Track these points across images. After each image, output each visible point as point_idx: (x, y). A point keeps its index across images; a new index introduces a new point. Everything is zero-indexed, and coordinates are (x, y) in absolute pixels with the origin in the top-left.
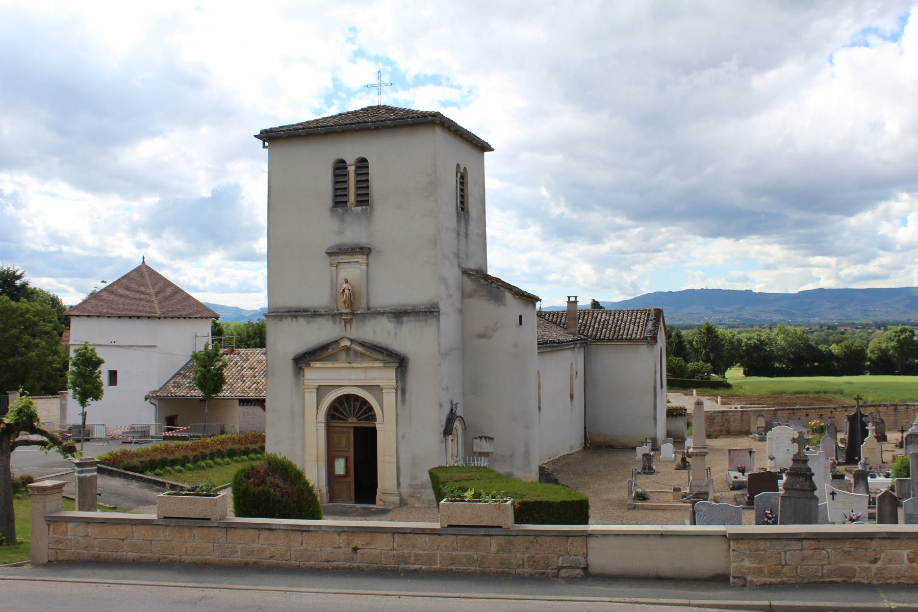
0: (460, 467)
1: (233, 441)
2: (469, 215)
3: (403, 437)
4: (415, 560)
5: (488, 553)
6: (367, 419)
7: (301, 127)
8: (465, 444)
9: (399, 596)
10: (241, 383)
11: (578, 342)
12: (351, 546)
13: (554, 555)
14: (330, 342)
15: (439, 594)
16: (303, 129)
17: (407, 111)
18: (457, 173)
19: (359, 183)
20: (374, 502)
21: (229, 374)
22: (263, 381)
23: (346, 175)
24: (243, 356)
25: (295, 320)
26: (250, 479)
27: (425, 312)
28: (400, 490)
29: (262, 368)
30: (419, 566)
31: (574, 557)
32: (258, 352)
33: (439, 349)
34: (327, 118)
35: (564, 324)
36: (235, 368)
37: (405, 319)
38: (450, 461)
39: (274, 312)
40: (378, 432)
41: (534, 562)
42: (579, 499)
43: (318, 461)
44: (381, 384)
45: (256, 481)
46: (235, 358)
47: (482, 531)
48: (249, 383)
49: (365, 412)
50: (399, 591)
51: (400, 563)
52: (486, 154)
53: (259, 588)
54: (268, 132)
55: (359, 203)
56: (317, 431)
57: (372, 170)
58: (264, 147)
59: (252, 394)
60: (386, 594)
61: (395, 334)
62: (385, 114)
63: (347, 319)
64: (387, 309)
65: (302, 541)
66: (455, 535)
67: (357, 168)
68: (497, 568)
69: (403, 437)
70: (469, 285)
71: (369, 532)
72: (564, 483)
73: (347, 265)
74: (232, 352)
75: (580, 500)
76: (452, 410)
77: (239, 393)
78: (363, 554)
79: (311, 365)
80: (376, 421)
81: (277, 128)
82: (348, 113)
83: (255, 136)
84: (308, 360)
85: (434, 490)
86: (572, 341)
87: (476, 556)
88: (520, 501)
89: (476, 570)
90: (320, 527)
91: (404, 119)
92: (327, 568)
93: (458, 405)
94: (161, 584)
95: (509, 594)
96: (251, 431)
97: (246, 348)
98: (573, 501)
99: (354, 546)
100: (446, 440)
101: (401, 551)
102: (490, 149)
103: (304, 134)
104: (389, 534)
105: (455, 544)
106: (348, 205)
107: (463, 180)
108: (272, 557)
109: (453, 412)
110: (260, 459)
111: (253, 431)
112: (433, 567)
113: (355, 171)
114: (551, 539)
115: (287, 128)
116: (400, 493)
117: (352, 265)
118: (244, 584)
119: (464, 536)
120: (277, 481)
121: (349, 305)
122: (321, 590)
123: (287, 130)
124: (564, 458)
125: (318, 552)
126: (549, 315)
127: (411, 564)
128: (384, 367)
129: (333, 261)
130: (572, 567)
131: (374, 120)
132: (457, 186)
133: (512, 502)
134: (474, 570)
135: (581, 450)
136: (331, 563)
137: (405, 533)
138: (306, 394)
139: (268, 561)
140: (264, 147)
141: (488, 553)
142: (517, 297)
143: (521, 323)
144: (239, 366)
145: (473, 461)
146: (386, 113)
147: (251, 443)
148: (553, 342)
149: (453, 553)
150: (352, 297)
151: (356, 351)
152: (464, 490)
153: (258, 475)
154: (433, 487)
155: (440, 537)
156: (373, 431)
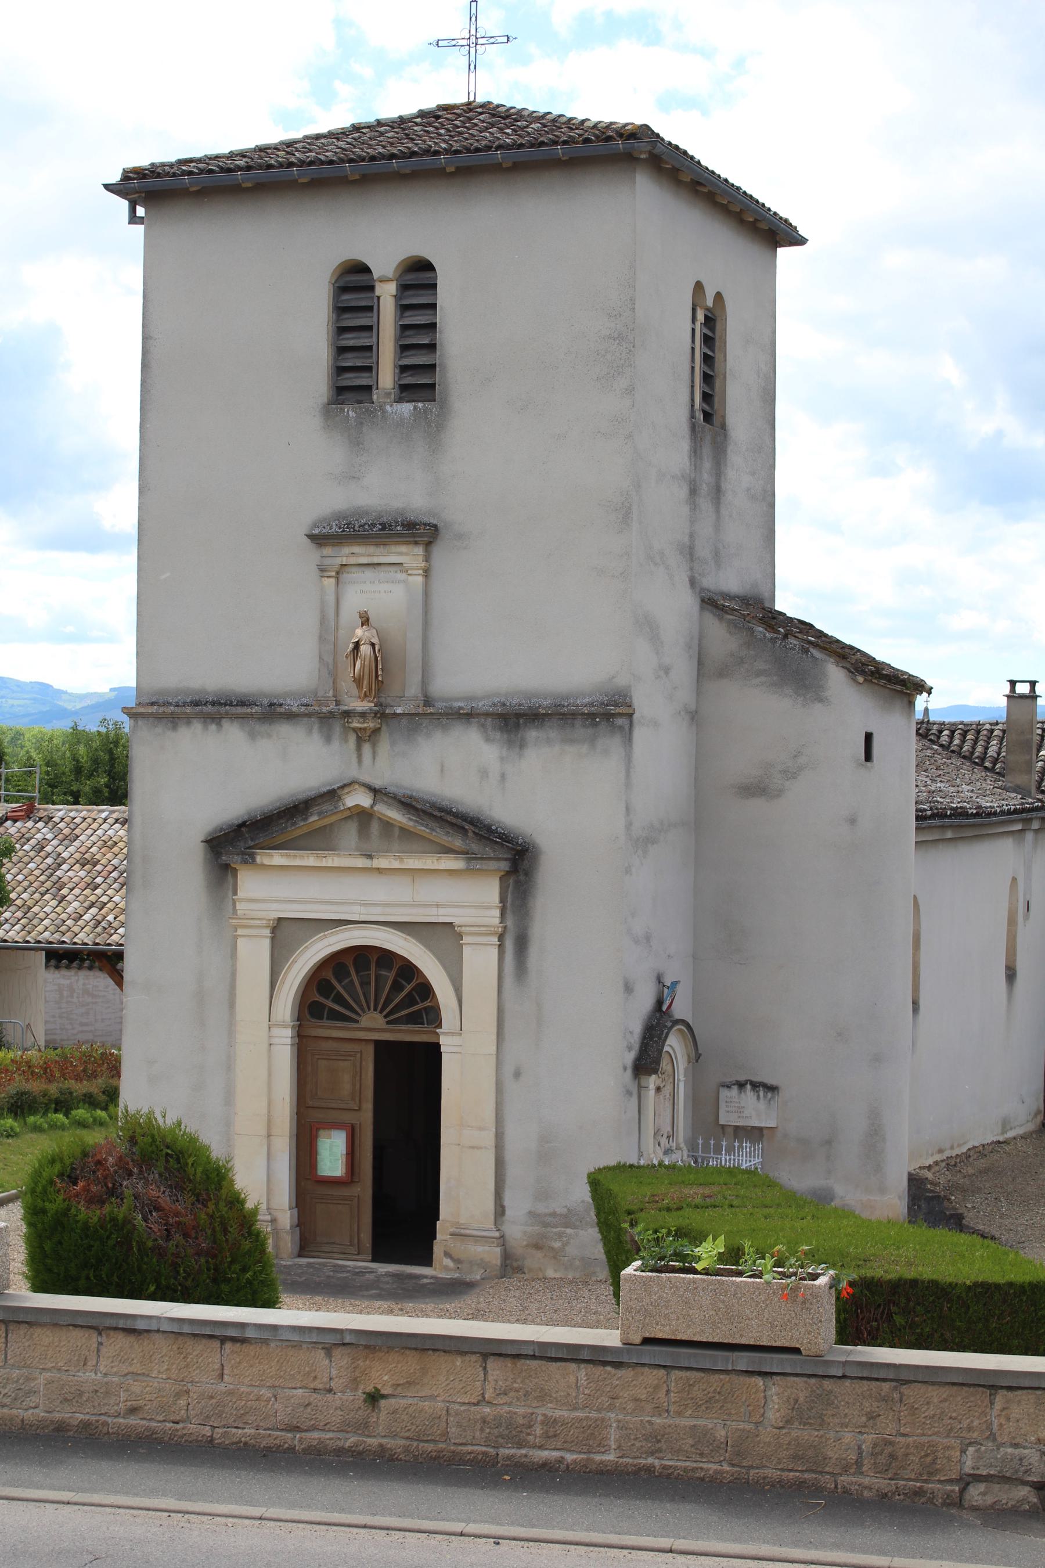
0: (680, 1169)
1: (28, 1069)
2: (725, 436)
3: (517, 1074)
4: (547, 1436)
5: (757, 1424)
6: (414, 1019)
7: (241, 163)
8: (696, 1101)
9: (497, 1540)
10: (54, 903)
11: (1034, 814)
12: (362, 1387)
13: (951, 1441)
14: (312, 793)
15: (614, 1539)
16: (249, 168)
17: (554, 121)
18: (694, 310)
19: (408, 333)
20: (427, 1259)
21: (20, 877)
22: (116, 899)
23: (370, 309)
24: (62, 825)
25: (213, 727)
26: (75, 1184)
27: (592, 716)
28: (503, 1228)
29: (115, 862)
30: (556, 1454)
31: (1010, 1450)
32: (106, 813)
33: (629, 826)
34: (318, 137)
35: (995, 761)
36: (38, 859)
37: (532, 734)
38: (651, 1151)
39: (153, 704)
40: (445, 1059)
41: (892, 1456)
42: (1028, 1278)
43: (269, 1136)
44: (456, 921)
45: (94, 1188)
46: (39, 830)
47: (743, 1361)
48: (76, 904)
49: (410, 1000)
50: (498, 1524)
51: (501, 1440)
52: (784, 254)
53: (96, 1498)
54: (144, 176)
55: (406, 392)
57: (447, 296)
58: (133, 219)
59: (84, 938)
60: (258, 1515)
61: (503, 776)
62: (487, 128)
63: (365, 729)
64: (482, 705)
65: (222, 1365)
66: (664, 1367)
67: (404, 288)
68: (782, 1470)
69: (517, 1074)
70: (718, 631)
71: (416, 1349)
72: (981, 1227)
73: (369, 573)
74: (29, 813)
75: (1030, 1283)
76: (660, 1002)
77: (47, 934)
78: (395, 1412)
79: (258, 859)
80: (440, 1026)
81: (171, 165)
82: (379, 123)
83: (107, 187)
84: (251, 843)
85: (601, 1232)
86: (1016, 812)
87: (723, 1433)
88: (854, 1276)
89: (721, 1472)
90: (275, 1328)
91: (542, 143)
92: (292, 1449)
93: (680, 989)
94: (86, 1500)
95: (817, 1548)
96: (80, 1043)
97: (68, 803)
98: (1011, 1284)
99: (370, 1389)
100: (640, 1087)
101: (506, 1408)
102: (796, 240)
103: (249, 185)
104: (474, 1358)
105: (662, 1394)
106: (375, 397)
107: (713, 329)
108: (133, 1411)
109: (664, 1008)
110: (102, 1124)
111: (87, 1042)
112: (598, 1458)
113: (397, 297)
114: (945, 1392)
115: (201, 166)
116: (502, 1236)
117: (382, 574)
118: (53, 1488)
119: (688, 1373)
120: (153, 1192)
121: (370, 689)
122: (272, 1512)
123: (201, 171)
124: (981, 1151)
125: (268, 1401)
126: (953, 732)
127: (534, 1447)
128: (468, 871)
129: (328, 561)
130: (1003, 1479)
131: (456, 146)
132: (693, 349)
133: (833, 1278)
134: (716, 1472)
135: (1031, 1133)
136: (303, 1435)
137: (518, 1356)
138: (241, 943)
139: (121, 1420)
140: (133, 219)
141: (757, 1424)
142: (861, 679)
143: (868, 757)
144: (48, 855)
145: (718, 1150)
146: (493, 125)
147: (78, 1078)
148: (960, 813)
149: (658, 1421)
150: (380, 667)
151: (388, 822)
152: (698, 1238)
153: (99, 1174)
154: (598, 1224)
155: (620, 1373)
156: (432, 1054)
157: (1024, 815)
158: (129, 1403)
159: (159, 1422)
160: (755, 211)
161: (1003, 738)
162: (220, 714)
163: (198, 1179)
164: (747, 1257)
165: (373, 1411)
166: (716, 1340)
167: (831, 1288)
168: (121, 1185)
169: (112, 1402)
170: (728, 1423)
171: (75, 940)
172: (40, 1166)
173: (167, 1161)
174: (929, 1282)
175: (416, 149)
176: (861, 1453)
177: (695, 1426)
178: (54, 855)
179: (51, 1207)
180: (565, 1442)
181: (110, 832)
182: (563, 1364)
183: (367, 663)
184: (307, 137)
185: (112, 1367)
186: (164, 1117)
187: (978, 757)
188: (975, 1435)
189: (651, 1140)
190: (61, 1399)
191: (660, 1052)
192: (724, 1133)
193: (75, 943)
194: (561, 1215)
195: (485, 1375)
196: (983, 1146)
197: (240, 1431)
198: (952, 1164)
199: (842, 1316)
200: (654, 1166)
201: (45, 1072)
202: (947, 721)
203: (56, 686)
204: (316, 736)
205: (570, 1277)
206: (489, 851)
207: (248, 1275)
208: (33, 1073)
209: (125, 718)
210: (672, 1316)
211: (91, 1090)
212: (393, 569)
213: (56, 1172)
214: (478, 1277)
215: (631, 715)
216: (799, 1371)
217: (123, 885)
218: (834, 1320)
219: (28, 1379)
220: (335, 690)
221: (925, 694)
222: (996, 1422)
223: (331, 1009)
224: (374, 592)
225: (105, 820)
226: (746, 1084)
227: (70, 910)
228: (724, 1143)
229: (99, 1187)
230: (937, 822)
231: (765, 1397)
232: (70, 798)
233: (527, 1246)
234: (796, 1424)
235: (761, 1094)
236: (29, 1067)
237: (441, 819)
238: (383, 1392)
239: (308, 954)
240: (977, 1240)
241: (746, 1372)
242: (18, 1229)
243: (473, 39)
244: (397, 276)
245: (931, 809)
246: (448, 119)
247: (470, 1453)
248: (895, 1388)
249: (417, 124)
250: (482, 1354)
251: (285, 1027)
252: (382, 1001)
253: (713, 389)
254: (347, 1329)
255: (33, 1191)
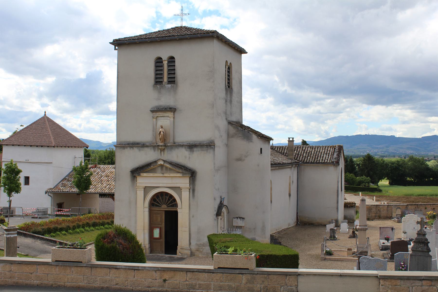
0: (225, 235)
3: (193, 217)
4: (199, 287)
5: (241, 284)
6: (173, 206)
7: (136, 38)
10: (101, 184)
11: (294, 164)
14: (152, 162)
16: (138, 39)
17: (198, 30)
18: (226, 66)
20: (176, 254)
21: (94, 179)
23: (162, 66)
24: (102, 169)
25: (132, 149)
27: (207, 145)
31: (290, 287)
33: (214, 167)
34: (152, 33)
35: (286, 154)
37: (195, 149)
39: (120, 144)
41: (267, 289)
42: (293, 254)
43: (144, 230)
45: (109, 240)
47: (238, 271)
49: (172, 202)
51: (190, 288)
52: (243, 55)
54: (117, 41)
55: (169, 82)
56: (144, 213)
57: (177, 64)
58: (115, 49)
59: (107, 191)
61: (189, 158)
62: (185, 31)
63: (162, 149)
64: (185, 144)
65: (134, 275)
66: (222, 273)
69: (193, 217)
70: (232, 130)
71: (173, 271)
73: (162, 118)
74: (95, 167)
75: (293, 255)
76: (221, 202)
78: (169, 283)
79: (141, 175)
80: (178, 207)
81: (123, 39)
82: (164, 30)
84: (140, 172)
85: (210, 247)
86: (290, 163)
87: (234, 285)
88: (259, 254)
90: (145, 267)
91: (195, 34)
97: (103, 165)
98: (290, 255)
99: (164, 279)
100: (217, 219)
101: (191, 282)
102: (245, 52)
103: (138, 42)
104: (184, 272)
105: (222, 278)
106: (163, 83)
108: (117, 284)
109: (222, 203)
110: (111, 228)
113: (167, 64)
114: (277, 276)
115: (129, 39)
116: (191, 249)
117: (165, 118)
119: (227, 274)
120: (121, 241)
123: (129, 40)
124: (284, 230)
125: (144, 282)
126: (278, 148)
127: (197, 289)
128: (183, 176)
131: (179, 35)
132: (226, 74)
133: (255, 255)
135: (295, 226)
136: (151, 288)
138: (138, 191)
139: (115, 286)
140: (115, 49)
141: (241, 284)
142: (259, 138)
143: (261, 153)
146: (186, 31)
147: (106, 219)
149: (221, 283)
150: (165, 136)
152: (228, 247)
154: (210, 246)
155: (214, 274)
156: (176, 213)
157: (292, 164)
158: (116, 283)
159: (122, 286)
160: (237, 47)
161: (287, 149)
162: (133, 146)
163: (130, 238)
164: (238, 251)
165: (165, 283)
166: (232, 267)
167: (255, 256)
168: (114, 240)
169: (113, 283)
170: (235, 283)
171: (95, 192)
172: (98, 236)
173: (123, 235)
174: (274, 255)
175: (171, 35)
176: (261, 289)
177: (228, 284)
178: (101, 175)
179: (100, 244)
180: (203, 288)
181: (112, 170)
182: (202, 273)
183: (162, 135)
184: (149, 33)
185: (113, 276)
186: (123, 226)
187: (283, 153)
188: (283, 284)
189: (220, 229)
190: (102, 282)
191: (221, 212)
192: (234, 227)
193: (105, 192)
194: (202, 244)
195: (187, 275)
196: (285, 229)
197: (138, 288)
198: (279, 233)
199: (257, 262)
200: (220, 234)
201: (99, 218)
202: (277, 146)
203: (101, 142)
204: (152, 150)
205: (204, 256)
206: (187, 172)
207: (140, 257)
208: (97, 218)
209: (114, 147)
210: (224, 263)
211: (108, 221)
212: (167, 117)
213: (101, 237)
214: (186, 257)
215: (214, 145)
216: (249, 273)
217: (114, 181)
218: (255, 263)
219: (96, 278)
220: (156, 141)
221: (272, 140)
222: (287, 282)
223: (156, 204)
224: (164, 122)
225: (111, 168)
226: (238, 218)
227: (104, 186)
228: (234, 229)
229: (110, 240)
230: (275, 165)
231: (242, 278)
232: (104, 164)
233: (196, 250)
234: (248, 283)
235: (241, 219)
236: (96, 217)
237: (175, 166)
238: (167, 279)
239: (151, 193)
240: (284, 247)
241: (238, 273)
242: (94, 249)
243: (182, 14)
244: (168, 59)
245: (274, 163)
246: (177, 29)
247: (184, 291)
248: (268, 276)
249: (171, 30)
250: (186, 271)
251: (147, 208)
252: (166, 202)
253: (230, 81)
254: (159, 267)
255: (96, 241)
